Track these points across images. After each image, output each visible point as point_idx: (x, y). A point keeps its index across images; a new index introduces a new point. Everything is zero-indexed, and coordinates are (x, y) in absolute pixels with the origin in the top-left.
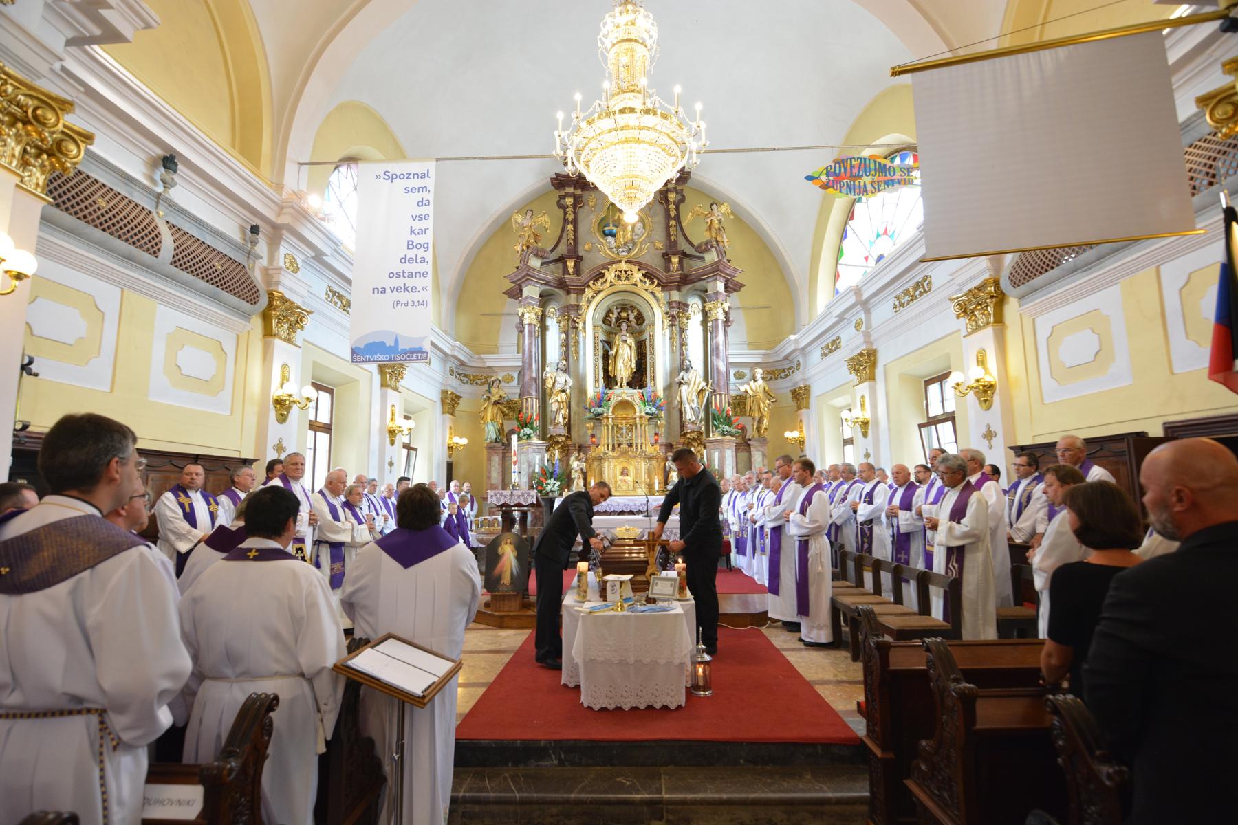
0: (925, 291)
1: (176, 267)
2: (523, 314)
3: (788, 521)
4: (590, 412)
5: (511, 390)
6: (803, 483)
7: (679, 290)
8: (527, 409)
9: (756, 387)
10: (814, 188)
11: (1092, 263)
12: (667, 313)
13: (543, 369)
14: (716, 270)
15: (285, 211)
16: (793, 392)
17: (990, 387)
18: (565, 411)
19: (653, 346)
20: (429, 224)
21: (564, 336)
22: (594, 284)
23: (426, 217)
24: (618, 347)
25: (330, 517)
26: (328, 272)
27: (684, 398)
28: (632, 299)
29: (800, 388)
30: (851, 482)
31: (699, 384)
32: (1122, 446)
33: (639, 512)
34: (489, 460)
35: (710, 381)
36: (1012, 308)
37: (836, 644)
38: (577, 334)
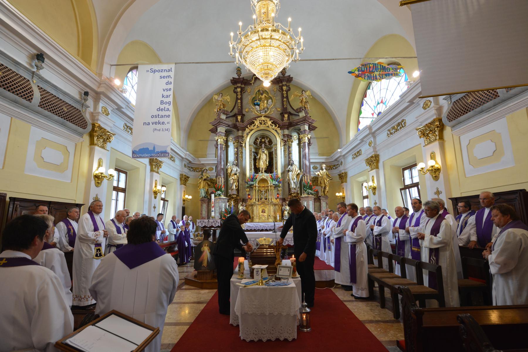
0: (403, 127)
1: (42, 108)
2: (218, 140)
3: (345, 235)
4: (248, 184)
5: (212, 174)
6: (352, 215)
7: (288, 129)
8: (219, 182)
9: (322, 173)
10: (352, 77)
11: (491, 108)
12: (282, 140)
13: (227, 164)
14: (305, 120)
15: (102, 85)
16: (339, 175)
17: (438, 170)
18: (236, 184)
19: (276, 154)
20: (171, 93)
21: (236, 149)
22: (250, 126)
23: (170, 89)
24: (261, 154)
25: (116, 233)
26: (125, 116)
27: (291, 178)
28: (267, 133)
29: (343, 173)
30: (371, 216)
31: (297, 171)
32: (512, 196)
33: (270, 230)
34: (202, 205)
35: (302, 170)
36: (448, 132)
37: (371, 298)
38: (242, 149)
